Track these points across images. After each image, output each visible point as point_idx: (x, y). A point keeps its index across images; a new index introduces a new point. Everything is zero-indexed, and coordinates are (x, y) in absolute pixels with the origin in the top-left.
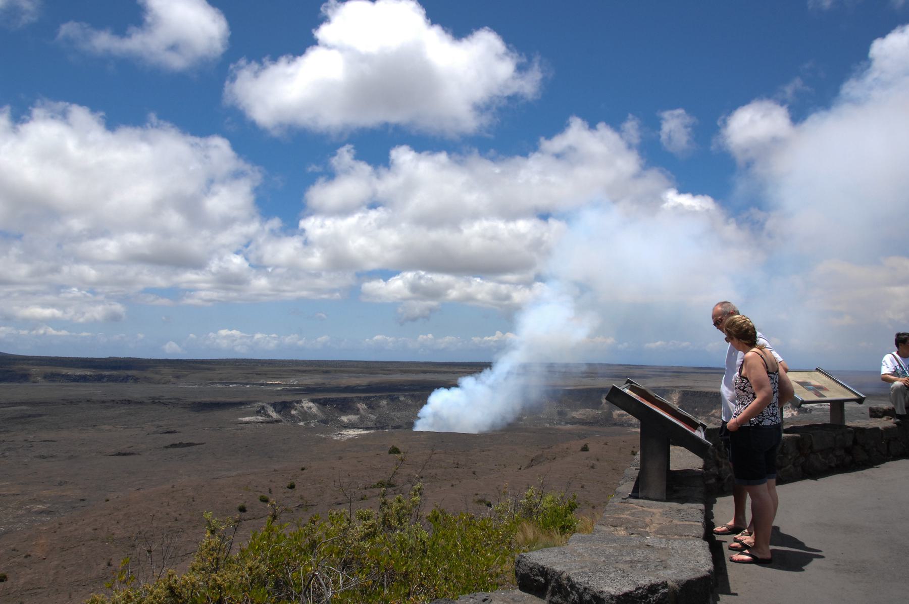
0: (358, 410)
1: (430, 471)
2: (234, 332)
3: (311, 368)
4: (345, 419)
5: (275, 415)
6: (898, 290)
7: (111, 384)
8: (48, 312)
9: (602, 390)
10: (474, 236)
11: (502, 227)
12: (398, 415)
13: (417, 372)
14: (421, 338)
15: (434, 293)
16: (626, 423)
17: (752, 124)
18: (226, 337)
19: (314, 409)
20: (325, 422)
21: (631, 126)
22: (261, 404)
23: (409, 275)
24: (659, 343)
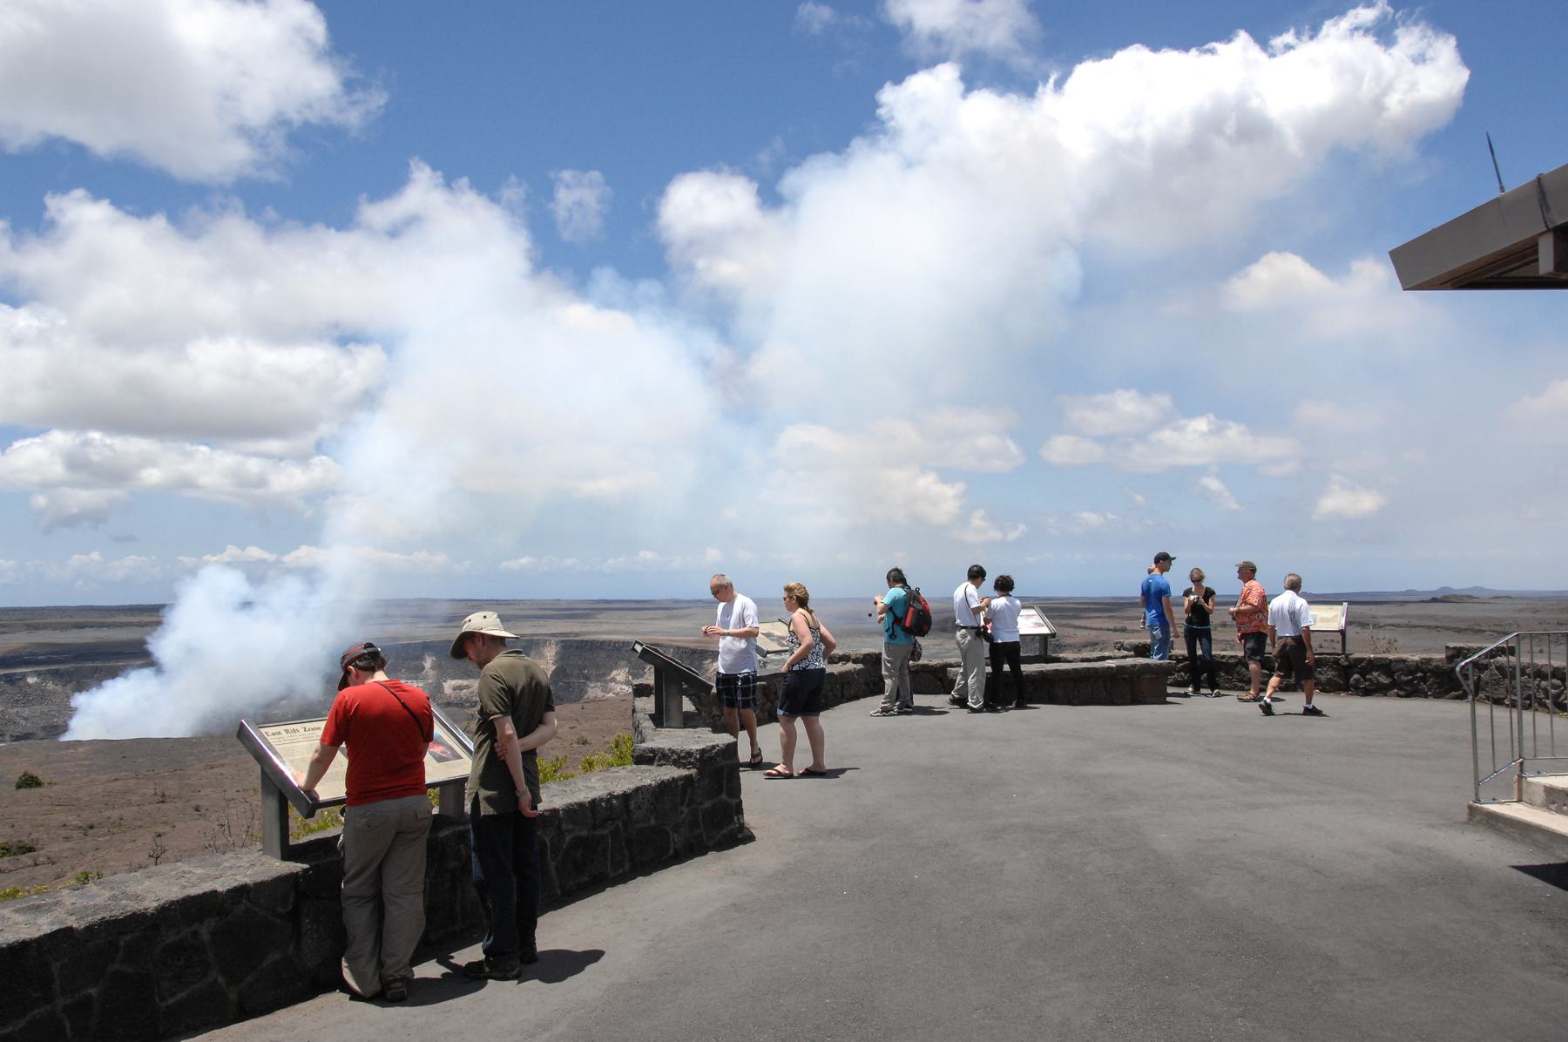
1: (107, 813)
9: (427, 647)
10: (212, 366)
11: (269, 358)
12: (26, 712)
13: (63, 627)
14: (76, 559)
15: (114, 474)
16: (467, 700)
17: (700, 203)
21: (513, 192)
24: (524, 560)
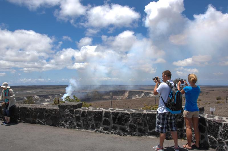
0: (50, 98)
4: (46, 100)
19: (38, 97)
20: (41, 101)
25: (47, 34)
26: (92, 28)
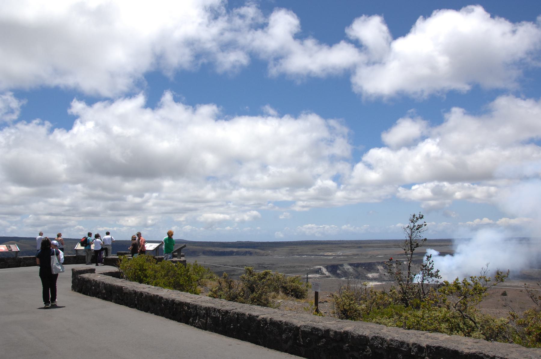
0: (378, 270)
2: (313, 225)
3: (351, 245)
4: (370, 275)
5: (327, 274)
6: (155, 208)
7: (238, 257)
8: (221, 216)
18: (309, 228)
22: (319, 267)
23: (431, 185)
25: (383, 14)
26: (219, 8)
